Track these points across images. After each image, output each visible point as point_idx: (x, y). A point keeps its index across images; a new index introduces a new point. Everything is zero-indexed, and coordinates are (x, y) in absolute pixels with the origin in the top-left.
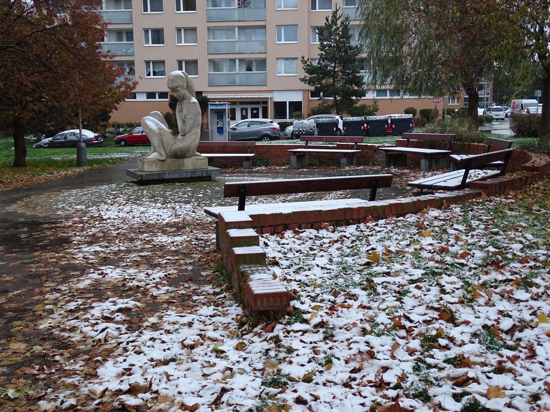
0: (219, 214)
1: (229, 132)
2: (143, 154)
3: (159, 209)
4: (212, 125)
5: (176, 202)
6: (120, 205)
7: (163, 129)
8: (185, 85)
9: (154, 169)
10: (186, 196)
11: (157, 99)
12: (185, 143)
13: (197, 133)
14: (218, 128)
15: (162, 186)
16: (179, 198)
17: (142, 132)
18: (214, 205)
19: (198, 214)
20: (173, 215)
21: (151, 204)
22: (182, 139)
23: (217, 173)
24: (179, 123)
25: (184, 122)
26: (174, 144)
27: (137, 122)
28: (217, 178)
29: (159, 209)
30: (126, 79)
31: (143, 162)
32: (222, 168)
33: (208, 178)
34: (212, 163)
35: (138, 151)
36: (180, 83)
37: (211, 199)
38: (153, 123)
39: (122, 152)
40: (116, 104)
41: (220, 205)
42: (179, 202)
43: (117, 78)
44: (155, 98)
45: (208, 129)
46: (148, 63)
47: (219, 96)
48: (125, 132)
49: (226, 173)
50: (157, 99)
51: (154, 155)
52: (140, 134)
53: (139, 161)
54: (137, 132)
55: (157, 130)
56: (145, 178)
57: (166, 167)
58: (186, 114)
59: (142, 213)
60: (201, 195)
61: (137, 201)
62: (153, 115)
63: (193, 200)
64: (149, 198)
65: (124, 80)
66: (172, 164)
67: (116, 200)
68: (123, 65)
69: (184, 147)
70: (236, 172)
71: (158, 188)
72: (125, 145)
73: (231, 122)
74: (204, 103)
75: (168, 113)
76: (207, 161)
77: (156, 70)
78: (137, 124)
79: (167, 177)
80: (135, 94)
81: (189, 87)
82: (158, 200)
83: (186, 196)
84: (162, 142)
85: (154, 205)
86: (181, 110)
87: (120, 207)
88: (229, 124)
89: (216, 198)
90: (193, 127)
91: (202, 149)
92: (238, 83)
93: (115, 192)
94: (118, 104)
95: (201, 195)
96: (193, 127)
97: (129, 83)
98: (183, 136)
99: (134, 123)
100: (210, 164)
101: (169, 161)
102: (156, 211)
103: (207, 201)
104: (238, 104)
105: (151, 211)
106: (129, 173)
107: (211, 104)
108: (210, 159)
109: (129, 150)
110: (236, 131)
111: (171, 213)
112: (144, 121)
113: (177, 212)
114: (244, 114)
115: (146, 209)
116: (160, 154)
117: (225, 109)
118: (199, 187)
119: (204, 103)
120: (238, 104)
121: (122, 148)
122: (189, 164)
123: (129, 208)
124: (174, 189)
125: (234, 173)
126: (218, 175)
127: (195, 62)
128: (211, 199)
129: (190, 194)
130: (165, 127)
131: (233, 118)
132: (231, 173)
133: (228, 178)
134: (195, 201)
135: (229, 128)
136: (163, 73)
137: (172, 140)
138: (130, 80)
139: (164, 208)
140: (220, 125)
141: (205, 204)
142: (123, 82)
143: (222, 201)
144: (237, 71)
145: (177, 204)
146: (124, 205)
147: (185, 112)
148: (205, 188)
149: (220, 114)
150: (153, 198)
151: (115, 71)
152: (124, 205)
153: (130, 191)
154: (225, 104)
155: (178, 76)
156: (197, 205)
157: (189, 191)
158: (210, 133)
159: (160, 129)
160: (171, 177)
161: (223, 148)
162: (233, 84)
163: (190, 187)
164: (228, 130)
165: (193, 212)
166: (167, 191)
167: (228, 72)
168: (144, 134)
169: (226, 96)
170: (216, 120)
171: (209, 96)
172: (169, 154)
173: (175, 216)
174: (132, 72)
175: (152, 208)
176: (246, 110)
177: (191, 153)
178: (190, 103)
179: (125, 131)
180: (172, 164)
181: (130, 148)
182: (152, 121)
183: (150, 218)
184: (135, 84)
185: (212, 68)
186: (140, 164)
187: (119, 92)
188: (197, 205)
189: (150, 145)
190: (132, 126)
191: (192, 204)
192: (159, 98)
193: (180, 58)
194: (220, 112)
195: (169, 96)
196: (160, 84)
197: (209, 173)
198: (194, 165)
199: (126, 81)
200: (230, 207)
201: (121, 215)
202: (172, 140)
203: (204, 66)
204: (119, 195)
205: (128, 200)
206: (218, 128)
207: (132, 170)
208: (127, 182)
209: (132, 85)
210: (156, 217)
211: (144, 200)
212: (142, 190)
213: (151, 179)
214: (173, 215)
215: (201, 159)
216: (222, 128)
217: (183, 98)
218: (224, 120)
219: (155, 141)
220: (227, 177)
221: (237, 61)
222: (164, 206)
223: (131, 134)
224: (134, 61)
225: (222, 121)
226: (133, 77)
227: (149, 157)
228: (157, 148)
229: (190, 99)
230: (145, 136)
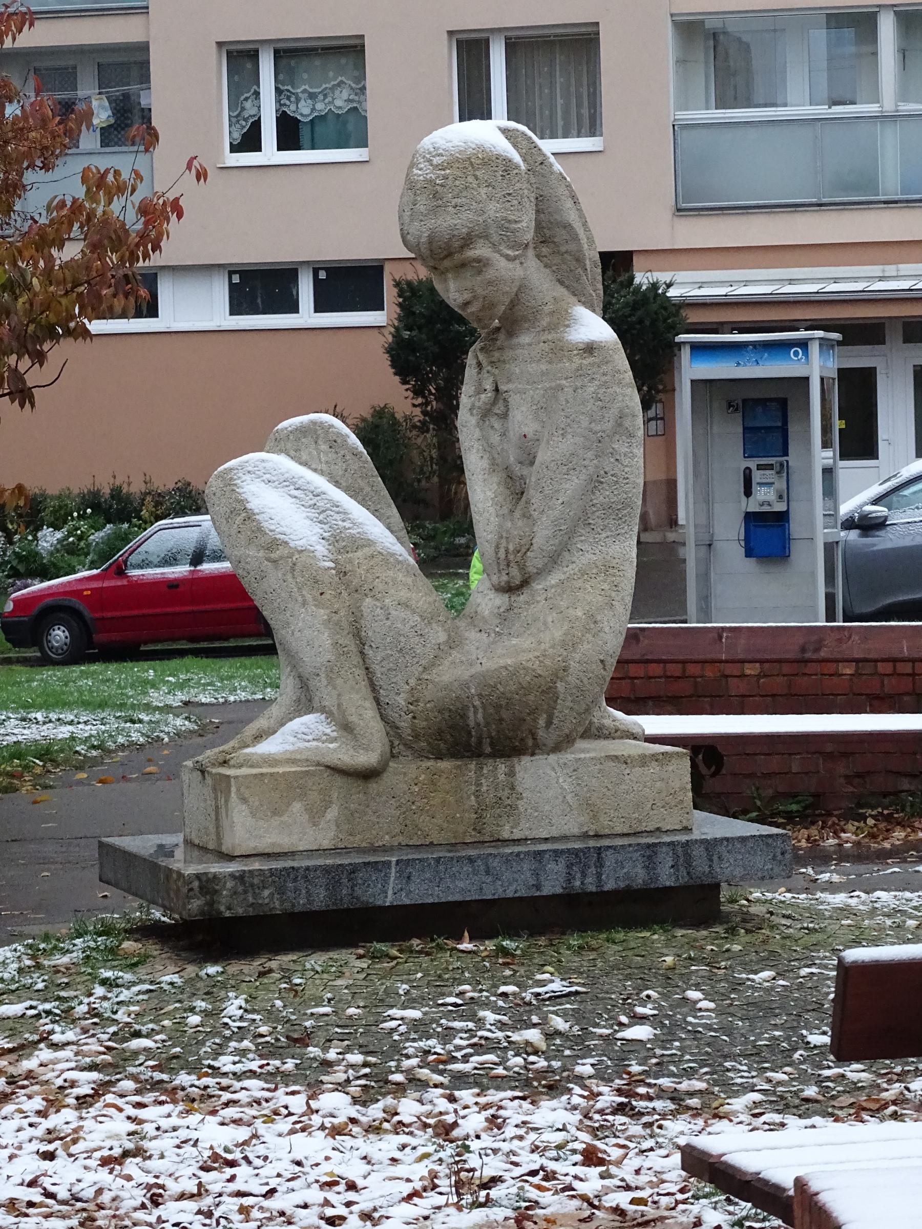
0: (800, 1183)
1: (830, 548)
2: (218, 724)
3: (336, 1131)
4: (705, 496)
5: (460, 1080)
6: (53, 1104)
7: (360, 543)
8: (526, 222)
9: (300, 833)
10: (533, 1035)
11: (307, 315)
12: (526, 642)
13: (607, 569)
14: (751, 518)
15: (353, 962)
16: (478, 1048)
17: (198, 558)
18: (739, 1104)
19: (626, 1172)
20: (444, 1184)
21: (281, 1097)
22: (505, 616)
23: (760, 861)
24: (483, 493)
25: (516, 490)
26: (441, 652)
27: (165, 482)
28: (759, 896)
29: (336, 1131)
30: (99, 184)
31: (222, 785)
32: (790, 819)
33: (689, 902)
34: (711, 785)
35: (169, 694)
36: (493, 209)
37: (715, 1058)
38: (295, 501)
39: (53, 701)
40: (25, 363)
41: (790, 1104)
42: (482, 1081)
43: (29, 177)
44: (293, 307)
45: (673, 522)
46: (241, 59)
47: (757, 282)
48: (73, 551)
49: (821, 859)
50: (307, 315)
51: (296, 737)
52: (182, 570)
53: (188, 777)
54: (164, 549)
55: (321, 549)
56: (230, 905)
57: (382, 820)
58: (530, 428)
59: (217, 1161)
60: (641, 1032)
61: (176, 1072)
62: (292, 445)
63: (585, 1068)
64: (267, 1051)
65: (80, 192)
66: (429, 798)
67: (29, 1064)
68: (69, 77)
69: (513, 673)
70: (898, 854)
71: (329, 978)
72: (75, 655)
73: (850, 472)
74: (650, 330)
75: (381, 413)
76: (680, 771)
77: (303, 110)
78: (159, 499)
79: (390, 893)
80: (151, 280)
81: (551, 236)
82: (327, 1065)
83: (533, 1035)
84: (357, 635)
85: (298, 1103)
86: (497, 405)
87: (54, 1120)
88: (830, 491)
89: (755, 1055)
90: (581, 521)
91: (645, 680)
92: (890, 182)
93: (15, 1009)
94: (40, 358)
95: (641, 1032)
96: (581, 521)
97: (116, 206)
98: (509, 589)
99: (136, 488)
100: (703, 798)
101: (408, 773)
102: (314, 1146)
103: (689, 1074)
104: (894, 337)
105: (280, 1146)
106: (120, 868)
107: (698, 349)
108: (704, 751)
109: (107, 691)
110: (885, 541)
111: (422, 1169)
112: (229, 483)
113: (473, 1161)
115: (243, 1133)
116: (346, 728)
117: (805, 381)
118: (623, 967)
119: (650, 330)
120: (894, 337)
121: (51, 676)
122: (551, 797)
123: (120, 1125)
124: (440, 984)
125: (882, 856)
126: (766, 879)
128: (715, 1058)
129: (559, 1023)
130: (379, 530)
131: (860, 442)
132: (860, 856)
133: (839, 899)
134: (601, 1075)
135: (831, 515)
136: (348, 129)
137: (429, 619)
138: (121, 189)
139: (374, 1129)
140: (765, 496)
141: (675, 1097)
142: (77, 207)
143: (804, 1078)
144: (889, 102)
145: (466, 1095)
146: (83, 1102)
147: (522, 419)
148: (669, 979)
149: (764, 418)
150: (293, 1053)
151: (20, 130)
152: (83, 1102)
153: (124, 998)
154: (803, 344)
155: (480, 162)
156: (620, 1109)
157: (556, 998)
158: (690, 554)
159: (345, 543)
160: (423, 891)
161: (792, 673)
162: (857, 194)
163: (564, 972)
164: (822, 533)
165: (591, 1157)
166: (388, 1000)
167: (822, 110)
168: (208, 567)
169: (808, 280)
170: (732, 459)
171: (684, 285)
172: (404, 723)
173: (459, 1186)
174: (131, 124)
175: (284, 1125)
177: (564, 709)
178: (560, 350)
179: (72, 550)
180: (429, 798)
181: (110, 670)
182: (289, 483)
183: (274, 1204)
184: (159, 214)
185: (702, 78)
186: (195, 797)
187: (48, 275)
188: (620, 1109)
189: (271, 650)
190: (122, 510)
191: (577, 1095)
192: (320, 307)
193: (473, 20)
194: (763, 402)
195: (390, 294)
196: (336, 204)
197: (701, 866)
198: (590, 808)
199: (91, 195)
200: (873, 1128)
201: (65, 1175)
202: (429, 619)
203: (642, 75)
204: (45, 1024)
205: (113, 1066)
206: (751, 518)
207: (141, 844)
208: (106, 931)
209: (134, 223)
210: (315, 1195)
211: (226, 1063)
212: (214, 992)
213: (277, 906)
214: (444, 1184)
215: (644, 760)
216: (782, 517)
217: (513, 319)
218: (793, 459)
219: (306, 629)
220: (832, 888)
221: (887, 28)
222: (375, 1111)
223: (120, 570)
224: (144, 48)
225: (783, 469)
226: (142, 163)
227: (270, 747)
228: (320, 684)
229: (561, 320)
230: (229, 587)
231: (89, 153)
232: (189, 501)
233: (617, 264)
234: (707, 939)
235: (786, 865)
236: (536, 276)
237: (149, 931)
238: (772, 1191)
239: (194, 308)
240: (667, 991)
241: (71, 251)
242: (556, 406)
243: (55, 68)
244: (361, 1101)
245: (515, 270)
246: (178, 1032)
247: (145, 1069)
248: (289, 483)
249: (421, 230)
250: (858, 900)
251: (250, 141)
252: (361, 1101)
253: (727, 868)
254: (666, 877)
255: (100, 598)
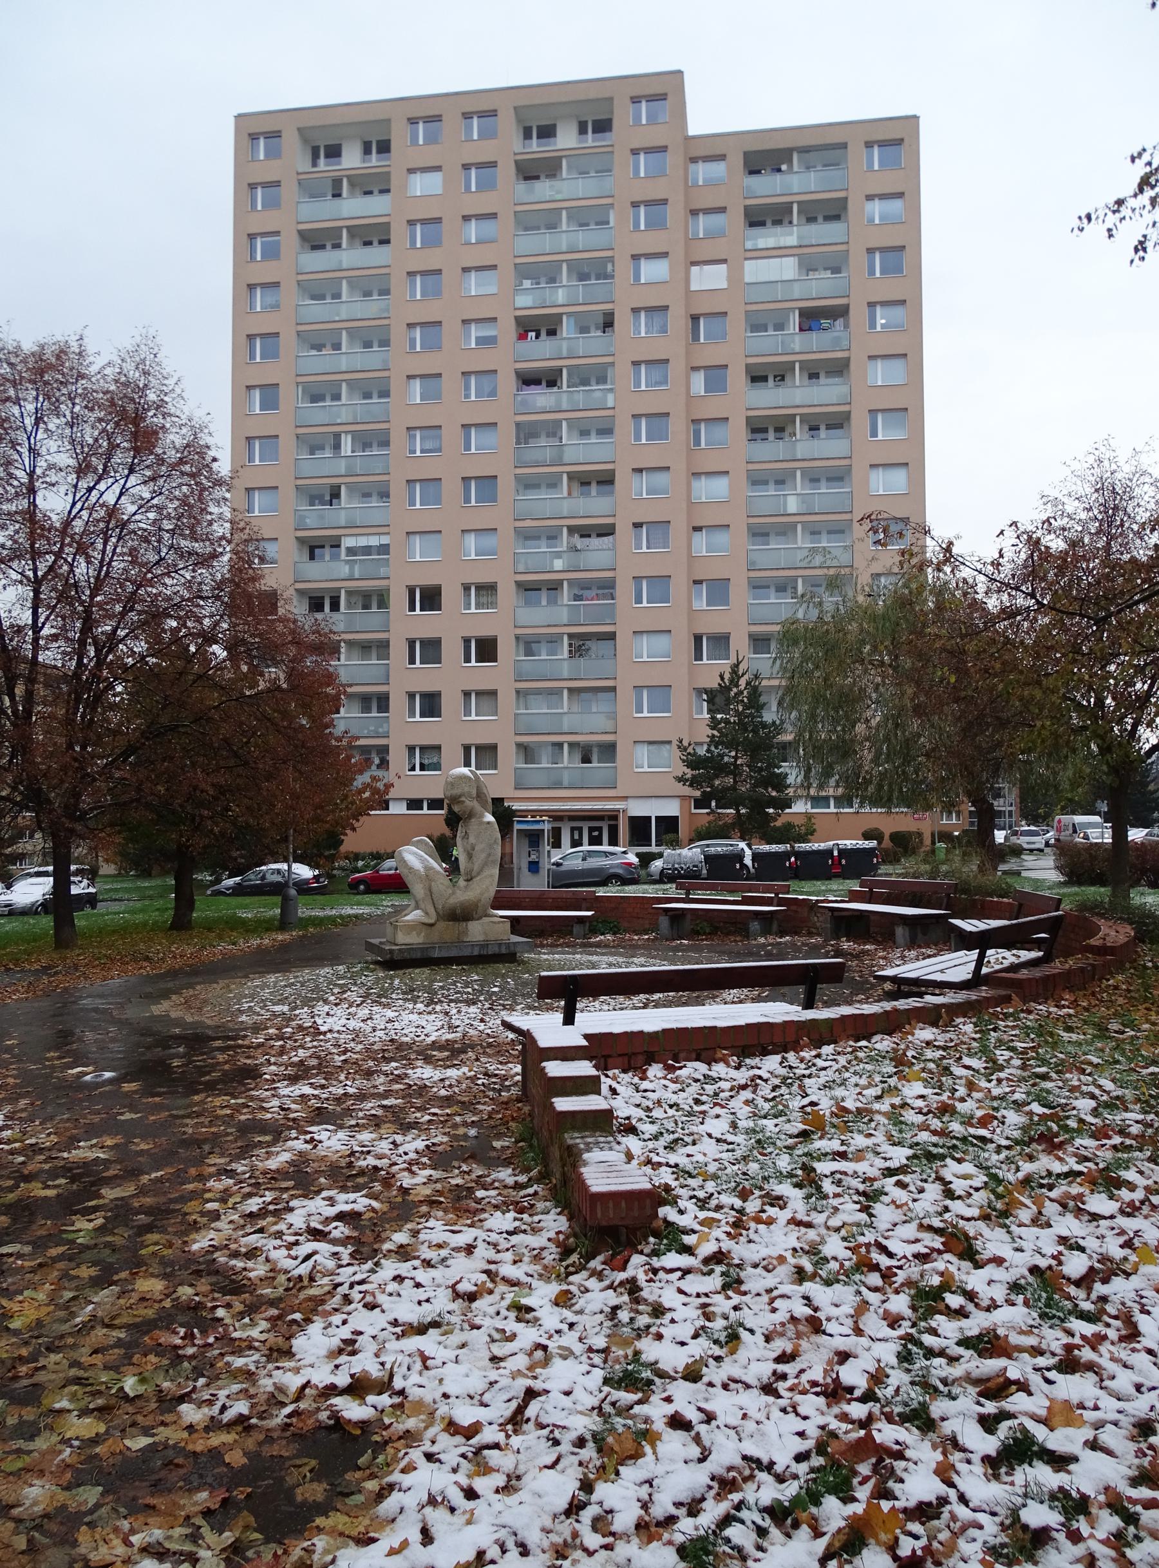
4: (519, 857)
6: (351, 1006)
7: (432, 868)
8: (474, 792)
9: (414, 939)
11: (425, 811)
15: (427, 971)
25: (470, 856)
30: (374, 778)
33: (509, 957)
35: (387, 902)
36: (466, 789)
37: (513, 996)
38: (416, 858)
39: (359, 904)
42: (456, 1001)
46: (411, 749)
48: (366, 867)
49: (542, 946)
50: (425, 811)
51: (415, 915)
54: (388, 867)
59: (390, 1021)
61: (381, 998)
62: (417, 844)
64: (404, 993)
71: (420, 975)
72: (366, 892)
73: (554, 851)
74: (505, 816)
76: (508, 925)
77: (426, 762)
81: (480, 796)
89: (523, 995)
90: (485, 864)
91: (500, 902)
96: (485, 864)
100: (514, 931)
101: (442, 925)
102: (414, 1017)
105: (406, 1017)
106: (370, 947)
108: (514, 920)
110: (562, 868)
114: (576, 837)
119: (505, 816)
121: (359, 897)
122: (476, 931)
124: (448, 977)
126: (529, 952)
127: (493, 748)
128: (513, 996)
131: (557, 844)
136: (437, 767)
140: (533, 857)
144: (566, 764)
147: (472, 840)
148: (503, 976)
150: (411, 994)
151: (355, 765)
153: (369, 979)
155: (463, 777)
159: (428, 869)
160: (444, 954)
161: (538, 901)
162: (558, 785)
164: (547, 866)
165: (482, 1021)
166: (435, 980)
170: (526, 848)
171: (516, 806)
174: (384, 764)
176: (580, 830)
177: (480, 910)
178: (482, 823)
180: (447, 931)
182: (415, 854)
185: (522, 757)
190: (379, 857)
196: (430, 785)
201: (352, 1024)
203: (508, 756)
205: (367, 996)
207: (376, 941)
212: (392, 978)
217: (471, 815)
219: (418, 889)
221: (566, 746)
229: (482, 816)
231: (374, 771)
232: (391, 856)
233: (498, 802)
234: (513, 966)
235: (532, 948)
236: (476, 805)
237: (377, 963)
238: (785, 990)
239: (398, 808)
240: (503, 980)
241: (367, 794)
242: (482, 836)
243: (365, 750)
244: (427, 1006)
245: (471, 804)
246: (382, 988)
247: (374, 997)
248: (415, 854)
249: (448, 794)
250: (550, 957)
251: (413, 769)
252: (427, 1006)
253: (518, 949)
254: (504, 951)
255: (372, 878)
